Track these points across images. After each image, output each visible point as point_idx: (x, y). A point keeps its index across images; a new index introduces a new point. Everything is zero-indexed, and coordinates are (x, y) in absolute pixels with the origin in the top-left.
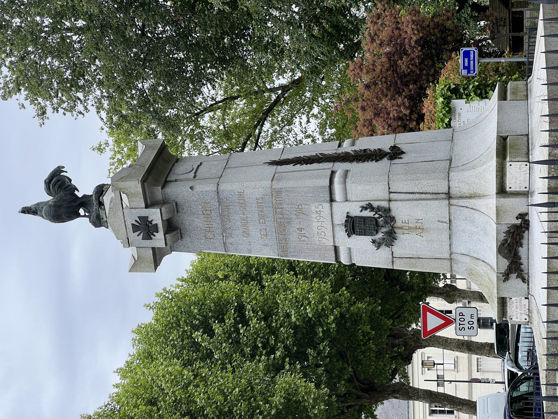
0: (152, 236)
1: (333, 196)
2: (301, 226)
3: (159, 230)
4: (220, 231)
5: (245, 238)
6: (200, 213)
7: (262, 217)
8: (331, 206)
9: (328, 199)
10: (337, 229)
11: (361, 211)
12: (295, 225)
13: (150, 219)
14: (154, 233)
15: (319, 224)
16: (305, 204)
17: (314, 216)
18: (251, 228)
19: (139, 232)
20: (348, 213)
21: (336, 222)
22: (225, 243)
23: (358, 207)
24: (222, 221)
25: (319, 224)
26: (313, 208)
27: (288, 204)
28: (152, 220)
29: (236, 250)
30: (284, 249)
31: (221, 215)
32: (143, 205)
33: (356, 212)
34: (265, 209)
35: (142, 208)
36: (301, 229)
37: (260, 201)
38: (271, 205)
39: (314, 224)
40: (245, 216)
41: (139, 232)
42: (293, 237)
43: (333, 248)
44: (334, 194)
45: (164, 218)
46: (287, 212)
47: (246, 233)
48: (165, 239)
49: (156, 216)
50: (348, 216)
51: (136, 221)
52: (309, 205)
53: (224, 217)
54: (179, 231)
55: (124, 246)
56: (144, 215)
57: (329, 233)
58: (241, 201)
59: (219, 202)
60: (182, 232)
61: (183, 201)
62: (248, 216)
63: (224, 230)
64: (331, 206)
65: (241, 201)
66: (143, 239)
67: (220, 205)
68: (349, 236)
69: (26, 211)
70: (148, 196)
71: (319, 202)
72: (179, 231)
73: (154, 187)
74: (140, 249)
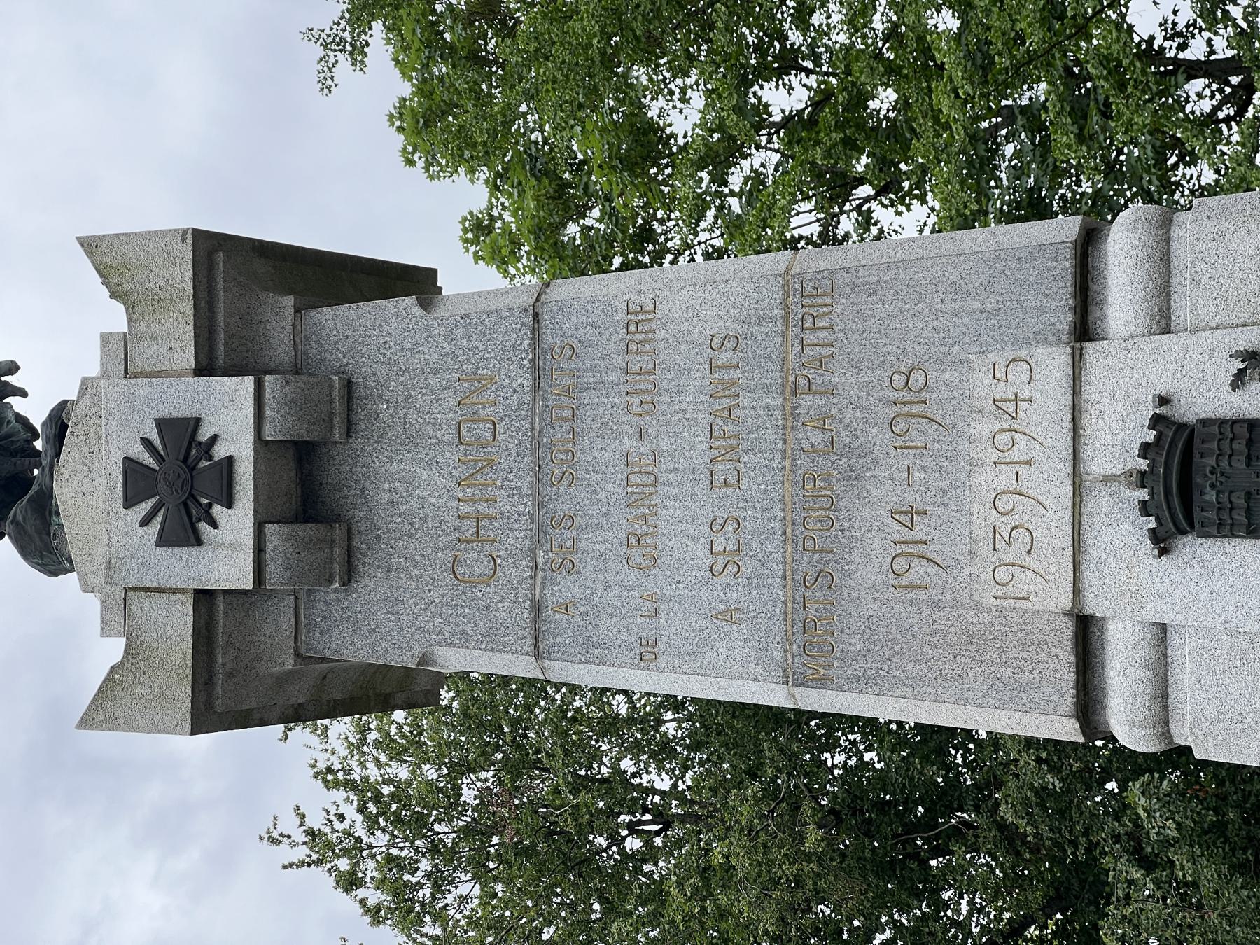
0: (204, 527)
1: (1095, 313)
2: (912, 496)
3: (238, 489)
4: (521, 536)
5: (632, 577)
6: (447, 434)
7: (727, 449)
8: (1078, 361)
9: (1065, 321)
10: (1101, 504)
11: (1238, 381)
12: (883, 491)
13: (204, 435)
14: (217, 510)
15: (1005, 478)
17: (982, 429)
18: (667, 514)
20: (1163, 401)
21: (1098, 463)
22: (537, 608)
23: (1222, 357)
25: (1005, 478)
26: (983, 384)
27: (857, 367)
28: (214, 439)
29: (586, 644)
30: (811, 651)
31: (536, 446)
32: (188, 359)
33: (1209, 395)
34: (744, 401)
35: (180, 374)
36: (910, 515)
37: (724, 357)
38: (774, 378)
39: (979, 479)
40: (646, 447)
42: (867, 565)
43: (1068, 627)
44: (1102, 303)
45: (269, 434)
46: (849, 414)
47: (642, 548)
48: (260, 549)
49: (231, 415)
50: (1156, 421)
51: (146, 442)
52: (963, 364)
55: (105, 624)
56: (182, 410)
57: (1054, 537)
58: (637, 362)
59: (536, 370)
60: (356, 542)
61: (381, 370)
62: (664, 444)
63: (539, 534)
64: (1078, 361)
65: (637, 362)
66: (161, 542)
67: (537, 386)
68: (1162, 543)
71: (1017, 343)
72: (339, 532)
73: (264, 296)
74: (145, 601)
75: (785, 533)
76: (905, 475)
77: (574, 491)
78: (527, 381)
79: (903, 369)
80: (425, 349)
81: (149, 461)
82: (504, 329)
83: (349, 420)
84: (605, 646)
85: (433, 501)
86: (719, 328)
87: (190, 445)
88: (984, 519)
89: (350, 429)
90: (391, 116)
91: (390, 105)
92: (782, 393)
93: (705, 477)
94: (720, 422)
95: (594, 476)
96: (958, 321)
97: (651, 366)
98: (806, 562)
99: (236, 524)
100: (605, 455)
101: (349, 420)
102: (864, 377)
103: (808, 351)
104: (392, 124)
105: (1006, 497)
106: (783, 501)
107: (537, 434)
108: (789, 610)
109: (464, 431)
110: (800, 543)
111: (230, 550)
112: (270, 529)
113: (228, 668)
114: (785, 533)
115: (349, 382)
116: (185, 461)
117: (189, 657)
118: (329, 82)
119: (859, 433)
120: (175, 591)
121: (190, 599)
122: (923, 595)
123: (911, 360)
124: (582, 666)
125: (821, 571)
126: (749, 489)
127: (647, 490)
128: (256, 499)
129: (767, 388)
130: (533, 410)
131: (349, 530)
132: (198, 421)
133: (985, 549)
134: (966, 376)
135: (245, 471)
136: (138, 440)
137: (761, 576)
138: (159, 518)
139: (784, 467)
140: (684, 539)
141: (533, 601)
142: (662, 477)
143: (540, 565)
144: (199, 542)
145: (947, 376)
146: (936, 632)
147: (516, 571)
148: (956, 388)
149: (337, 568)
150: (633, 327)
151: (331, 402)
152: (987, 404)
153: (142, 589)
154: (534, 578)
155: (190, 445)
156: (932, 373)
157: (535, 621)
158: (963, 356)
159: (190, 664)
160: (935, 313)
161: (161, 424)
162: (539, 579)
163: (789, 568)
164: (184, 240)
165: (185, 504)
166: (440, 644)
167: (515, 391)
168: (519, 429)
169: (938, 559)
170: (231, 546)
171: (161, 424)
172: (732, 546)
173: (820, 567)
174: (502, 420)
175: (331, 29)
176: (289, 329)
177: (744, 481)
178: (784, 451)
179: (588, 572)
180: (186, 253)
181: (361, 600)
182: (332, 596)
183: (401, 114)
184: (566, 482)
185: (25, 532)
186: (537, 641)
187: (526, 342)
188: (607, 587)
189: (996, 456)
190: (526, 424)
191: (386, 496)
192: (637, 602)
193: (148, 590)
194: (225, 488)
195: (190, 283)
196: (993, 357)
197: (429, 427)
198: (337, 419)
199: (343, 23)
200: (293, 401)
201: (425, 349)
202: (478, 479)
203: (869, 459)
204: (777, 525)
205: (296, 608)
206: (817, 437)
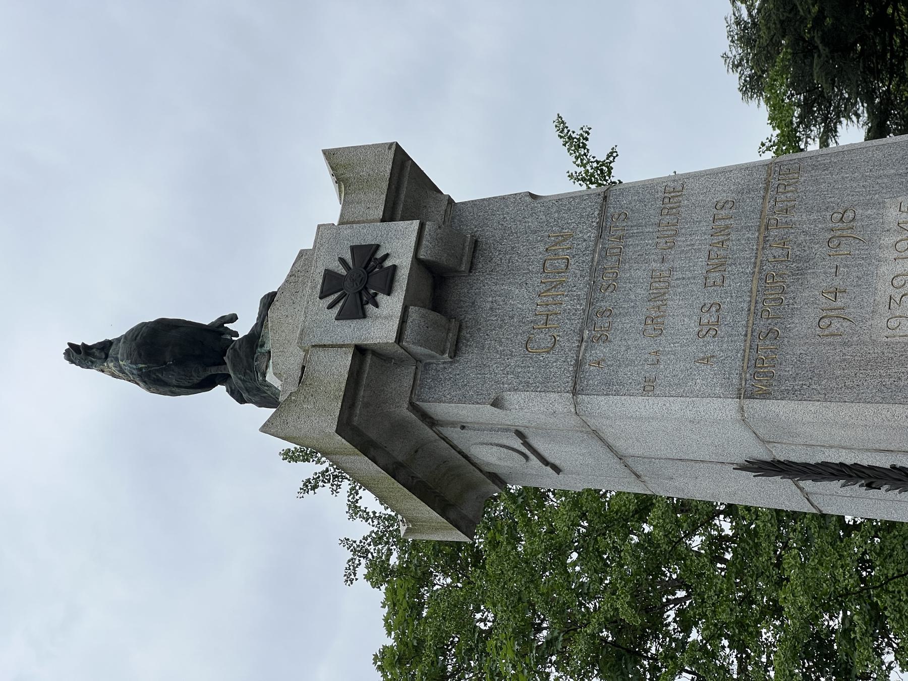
2: (837, 282)
3: (397, 285)
4: (577, 323)
6: (536, 267)
7: (719, 265)
13: (380, 254)
16: (867, 205)
17: (888, 240)
19: (351, 264)
22: (579, 364)
24: (593, 287)
28: (387, 256)
31: (593, 270)
32: (380, 213)
34: (733, 236)
38: (754, 222)
39: (883, 269)
41: (351, 264)
42: (802, 325)
45: (422, 255)
46: (802, 238)
47: (655, 324)
52: (882, 205)
53: (599, 279)
54: (454, 324)
56: (370, 240)
60: (464, 333)
61: (498, 234)
62: (676, 265)
63: (588, 320)
69: (80, 355)
70: (402, 197)
72: (454, 324)
74: (321, 353)
75: (749, 310)
76: (834, 270)
77: (614, 295)
78: (593, 234)
79: (840, 210)
80: (529, 220)
81: (343, 272)
82: (583, 206)
83: (472, 263)
84: (621, 384)
85: (520, 306)
86: (722, 197)
87: (370, 260)
88: (884, 290)
89: (472, 267)
90: (376, 656)
91: (377, 649)
92: (759, 230)
93: (701, 281)
94: (715, 249)
95: (629, 285)
96: (879, 181)
97: (675, 221)
98: (762, 325)
99: (391, 305)
100: (636, 280)
101: (472, 263)
102: (814, 216)
103: (779, 205)
104: (375, 663)
105: (899, 278)
106: (751, 291)
107: (595, 264)
108: (747, 354)
109: (547, 265)
110: (759, 314)
111: (382, 324)
112: (412, 309)
113: (365, 400)
114: (749, 310)
115: (476, 241)
116: (365, 268)
117: (344, 385)
118: (352, 577)
119: (806, 248)
120: (341, 346)
121: (351, 350)
122: (839, 339)
123: (847, 204)
124: (603, 398)
125: (771, 329)
126: (730, 286)
127: (662, 291)
128: (407, 290)
129: (748, 229)
130: (594, 251)
131: (460, 326)
132: (378, 247)
133: (883, 309)
134: (881, 211)
135: (403, 275)
136: (337, 259)
137: (731, 335)
138: (340, 304)
139: (754, 272)
140: (682, 319)
141: (577, 360)
142: (673, 283)
143: (585, 339)
144: (364, 316)
145: (869, 212)
146: (844, 360)
147: (568, 344)
148: (874, 219)
149: (448, 345)
150: (667, 200)
151: (463, 249)
152: (894, 226)
153: (320, 346)
154: (579, 347)
155: (370, 260)
156: (859, 211)
157: (576, 372)
158: (881, 200)
159: (343, 389)
160: (865, 178)
161: (353, 249)
162: (583, 347)
163: (750, 329)
164: (390, 148)
165: (360, 293)
166: (509, 390)
167: (585, 240)
168: (584, 262)
169: (851, 317)
170: (386, 318)
171: (353, 249)
172: (713, 319)
173: (771, 327)
174: (574, 257)
175: (361, 542)
176: (442, 212)
177: (727, 282)
178: (755, 263)
179: (616, 341)
180: (391, 155)
181: (461, 367)
182: (442, 366)
183: (383, 658)
184: (610, 290)
185: (238, 355)
186: (575, 384)
187: (596, 213)
188: (628, 348)
189: (896, 255)
190: (589, 258)
191: (488, 305)
192: (646, 356)
193: (325, 346)
194: (388, 282)
195: (389, 172)
196: (900, 199)
197: (525, 264)
198: (465, 259)
199: (369, 540)
200: (441, 239)
201: (529, 220)
202: (553, 292)
203: (811, 262)
204: (745, 306)
205: (415, 374)
206: (778, 252)
